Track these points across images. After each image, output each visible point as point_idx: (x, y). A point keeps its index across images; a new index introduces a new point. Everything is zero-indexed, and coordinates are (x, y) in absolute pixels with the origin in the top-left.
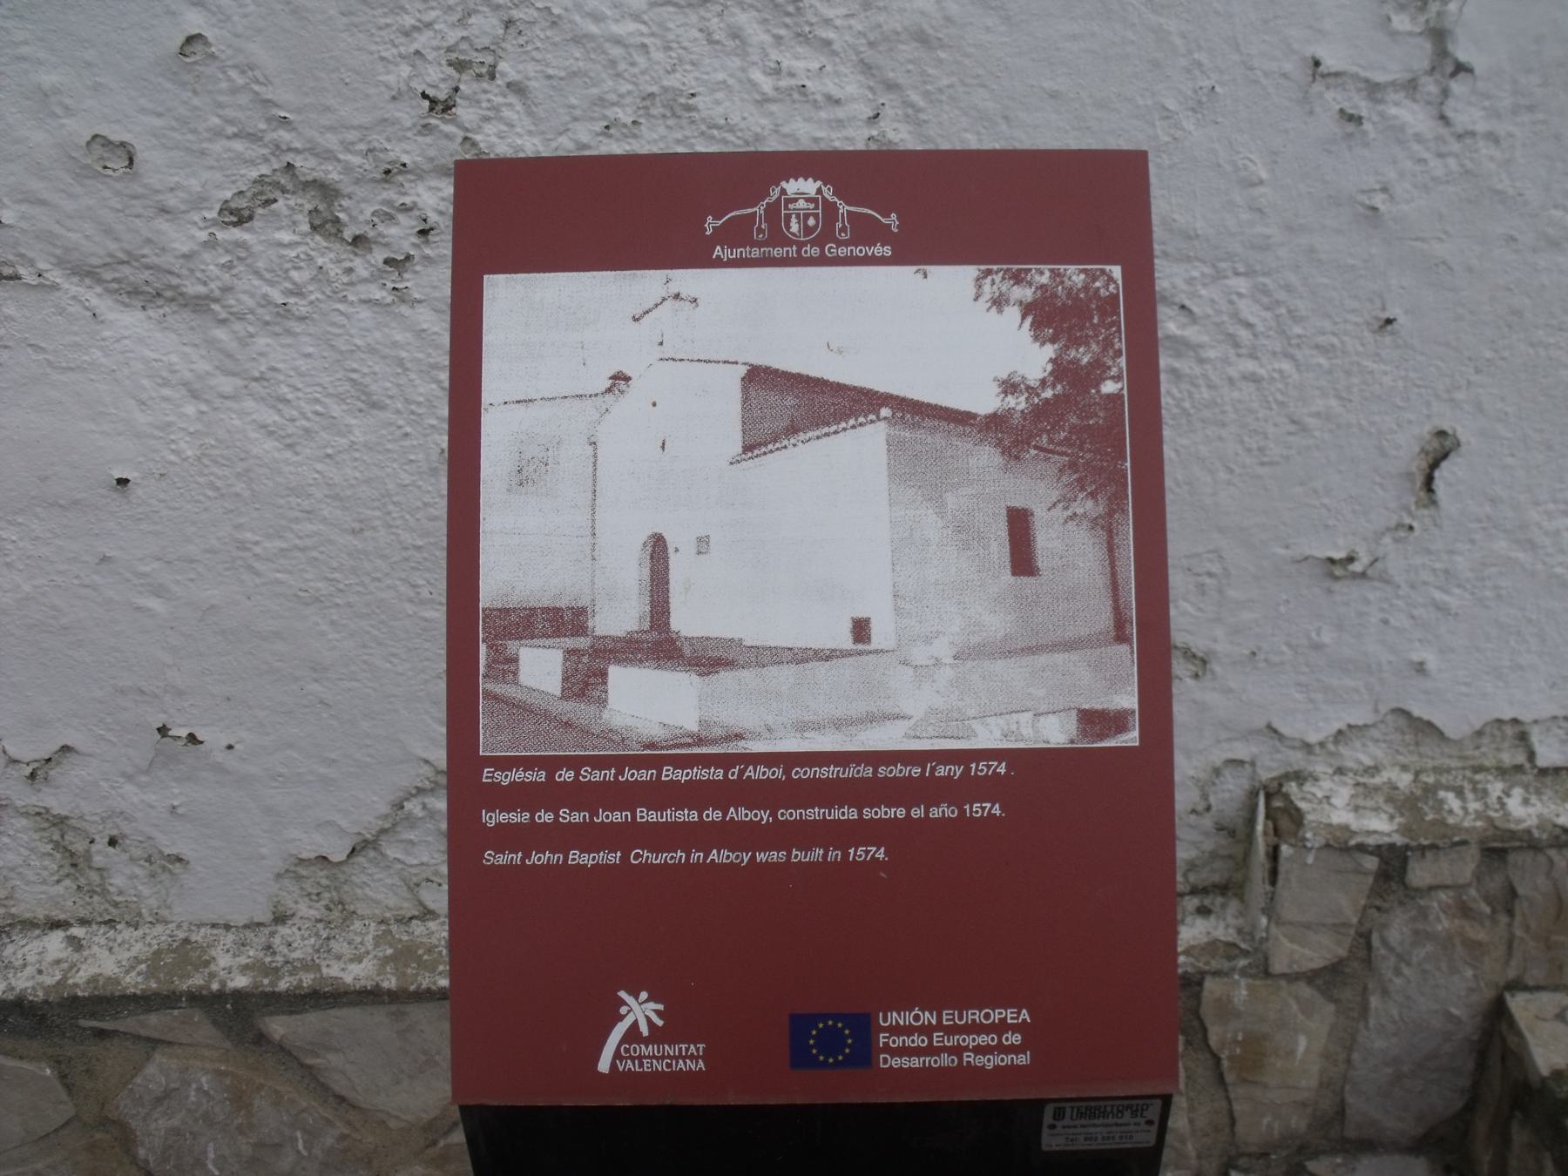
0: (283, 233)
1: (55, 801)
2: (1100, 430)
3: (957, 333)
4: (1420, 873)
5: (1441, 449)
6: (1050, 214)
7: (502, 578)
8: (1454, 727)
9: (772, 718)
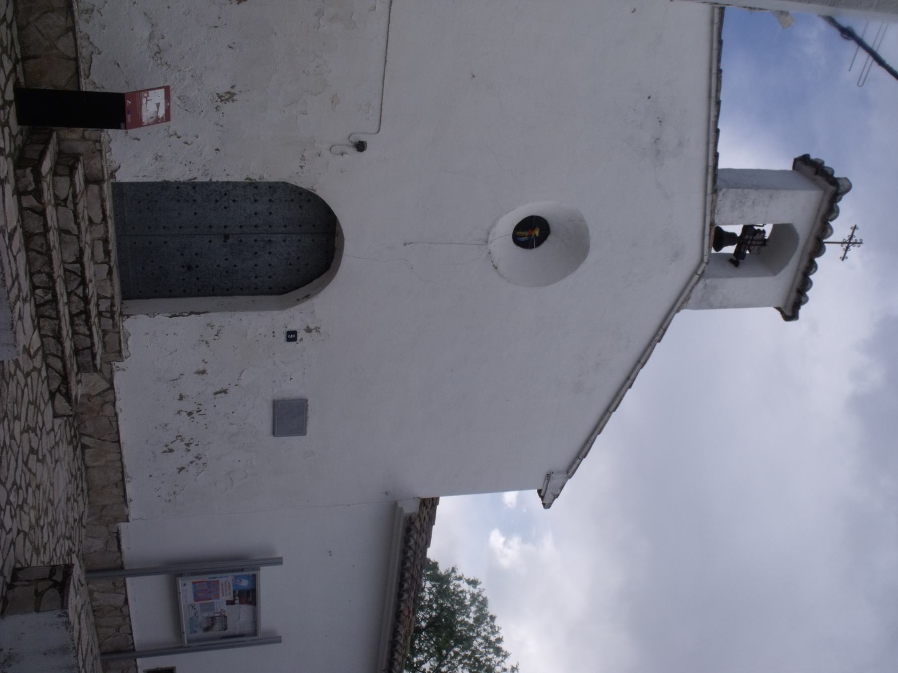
0: (156, 49)
1: (95, 12)
2: (157, 121)
3: (162, 113)
4: (97, 144)
5: (139, 140)
6: (167, 117)
7: (151, 93)
8: (111, 145)
9: (144, 107)
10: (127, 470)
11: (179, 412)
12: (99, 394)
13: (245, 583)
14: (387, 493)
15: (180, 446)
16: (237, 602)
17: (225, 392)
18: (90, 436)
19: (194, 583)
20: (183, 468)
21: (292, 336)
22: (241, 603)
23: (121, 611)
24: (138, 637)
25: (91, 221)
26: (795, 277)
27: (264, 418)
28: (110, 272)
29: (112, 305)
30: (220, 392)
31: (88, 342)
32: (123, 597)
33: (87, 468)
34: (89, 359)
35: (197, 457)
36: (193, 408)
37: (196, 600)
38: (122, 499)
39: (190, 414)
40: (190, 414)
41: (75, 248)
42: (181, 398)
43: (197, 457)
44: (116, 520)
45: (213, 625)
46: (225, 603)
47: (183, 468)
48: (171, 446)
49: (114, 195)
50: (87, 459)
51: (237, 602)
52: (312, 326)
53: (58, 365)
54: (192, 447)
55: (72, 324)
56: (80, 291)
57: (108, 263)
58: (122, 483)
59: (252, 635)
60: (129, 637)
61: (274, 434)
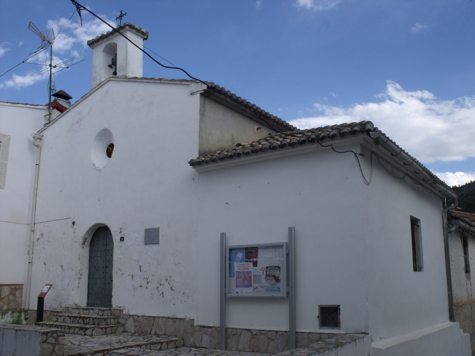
10: (170, 316)
11: (147, 288)
12: (135, 322)
13: (240, 255)
14: (193, 179)
15: (161, 288)
16: (255, 260)
17: (140, 267)
18: (151, 330)
19: (237, 287)
20: (171, 288)
21: (122, 239)
22: (256, 257)
23: (256, 335)
24: (286, 329)
25: (79, 313)
26: (101, 43)
27: (153, 248)
28: (92, 309)
29: (101, 310)
30: (140, 269)
31: (91, 319)
32: (244, 331)
33: (165, 334)
34: (96, 320)
35: (167, 281)
36: (145, 281)
37: (251, 286)
38: (181, 320)
39: (148, 283)
40: (148, 283)
41: (67, 318)
42: (141, 286)
43: (167, 281)
44: (193, 326)
45: (273, 276)
46: (255, 268)
47: (171, 288)
48: (161, 293)
49: (91, 306)
50: (161, 333)
51: (255, 260)
52: (120, 231)
53: (77, 330)
54: (162, 283)
55: (86, 324)
56: (78, 319)
57: (90, 309)
58: (175, 319)
59: (289, 250)
60: (279, 333)
61: (158, 243)
